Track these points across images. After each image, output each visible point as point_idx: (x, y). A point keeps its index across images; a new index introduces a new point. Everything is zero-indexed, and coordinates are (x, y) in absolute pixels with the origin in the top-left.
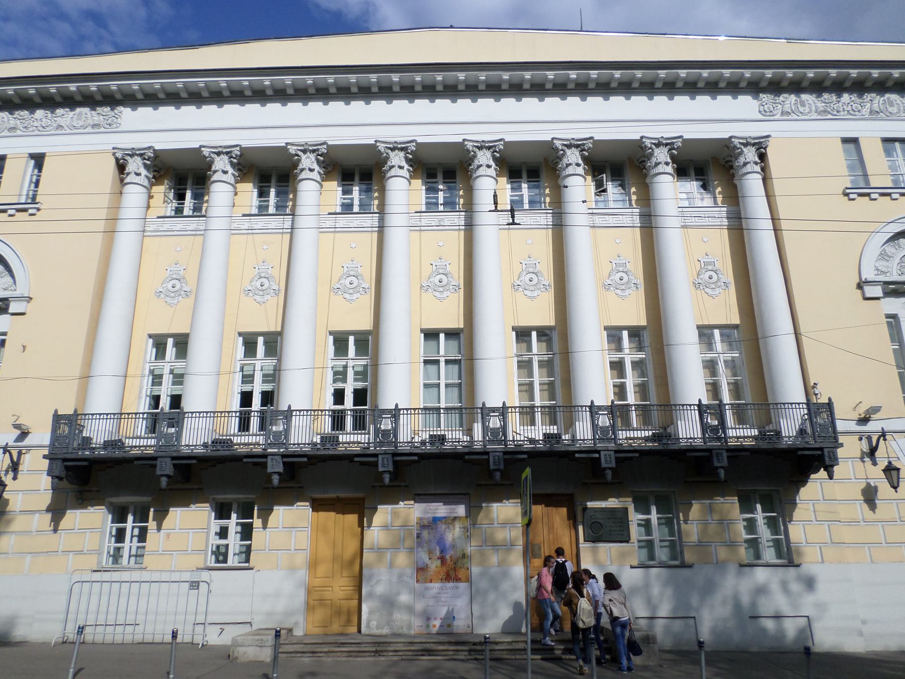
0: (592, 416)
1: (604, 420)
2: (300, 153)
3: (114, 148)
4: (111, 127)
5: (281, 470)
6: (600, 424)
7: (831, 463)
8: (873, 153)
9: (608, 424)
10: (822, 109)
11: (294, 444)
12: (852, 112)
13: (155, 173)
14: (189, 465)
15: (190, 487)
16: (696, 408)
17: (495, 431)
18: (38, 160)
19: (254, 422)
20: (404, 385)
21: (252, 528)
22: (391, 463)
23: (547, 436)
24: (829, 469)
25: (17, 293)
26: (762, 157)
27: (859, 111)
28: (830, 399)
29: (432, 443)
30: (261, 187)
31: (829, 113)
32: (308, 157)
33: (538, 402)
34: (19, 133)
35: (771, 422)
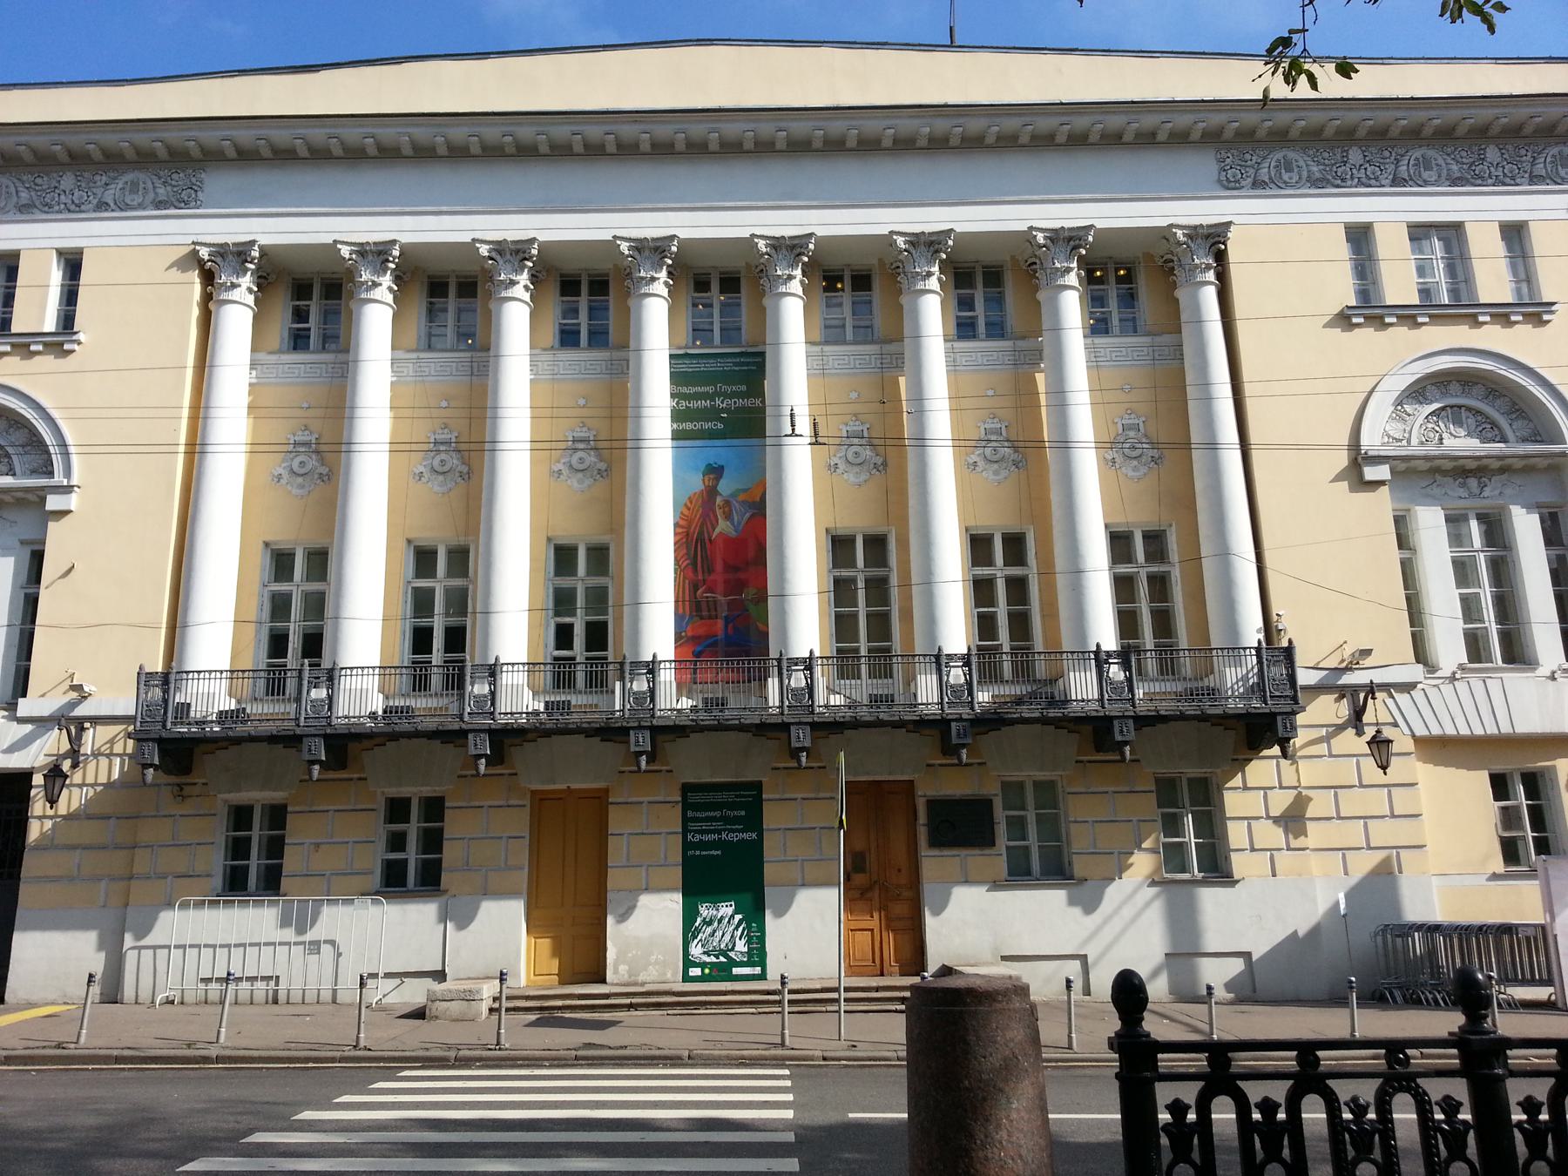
6: (952, 681)
8: (1392, 247)
10: (1318, 175)
15: (346, 776)
19: (436, 680)
23: (875, 700)
24: (1284, 743)
26: (1221, 257)
35: (1212, 672)
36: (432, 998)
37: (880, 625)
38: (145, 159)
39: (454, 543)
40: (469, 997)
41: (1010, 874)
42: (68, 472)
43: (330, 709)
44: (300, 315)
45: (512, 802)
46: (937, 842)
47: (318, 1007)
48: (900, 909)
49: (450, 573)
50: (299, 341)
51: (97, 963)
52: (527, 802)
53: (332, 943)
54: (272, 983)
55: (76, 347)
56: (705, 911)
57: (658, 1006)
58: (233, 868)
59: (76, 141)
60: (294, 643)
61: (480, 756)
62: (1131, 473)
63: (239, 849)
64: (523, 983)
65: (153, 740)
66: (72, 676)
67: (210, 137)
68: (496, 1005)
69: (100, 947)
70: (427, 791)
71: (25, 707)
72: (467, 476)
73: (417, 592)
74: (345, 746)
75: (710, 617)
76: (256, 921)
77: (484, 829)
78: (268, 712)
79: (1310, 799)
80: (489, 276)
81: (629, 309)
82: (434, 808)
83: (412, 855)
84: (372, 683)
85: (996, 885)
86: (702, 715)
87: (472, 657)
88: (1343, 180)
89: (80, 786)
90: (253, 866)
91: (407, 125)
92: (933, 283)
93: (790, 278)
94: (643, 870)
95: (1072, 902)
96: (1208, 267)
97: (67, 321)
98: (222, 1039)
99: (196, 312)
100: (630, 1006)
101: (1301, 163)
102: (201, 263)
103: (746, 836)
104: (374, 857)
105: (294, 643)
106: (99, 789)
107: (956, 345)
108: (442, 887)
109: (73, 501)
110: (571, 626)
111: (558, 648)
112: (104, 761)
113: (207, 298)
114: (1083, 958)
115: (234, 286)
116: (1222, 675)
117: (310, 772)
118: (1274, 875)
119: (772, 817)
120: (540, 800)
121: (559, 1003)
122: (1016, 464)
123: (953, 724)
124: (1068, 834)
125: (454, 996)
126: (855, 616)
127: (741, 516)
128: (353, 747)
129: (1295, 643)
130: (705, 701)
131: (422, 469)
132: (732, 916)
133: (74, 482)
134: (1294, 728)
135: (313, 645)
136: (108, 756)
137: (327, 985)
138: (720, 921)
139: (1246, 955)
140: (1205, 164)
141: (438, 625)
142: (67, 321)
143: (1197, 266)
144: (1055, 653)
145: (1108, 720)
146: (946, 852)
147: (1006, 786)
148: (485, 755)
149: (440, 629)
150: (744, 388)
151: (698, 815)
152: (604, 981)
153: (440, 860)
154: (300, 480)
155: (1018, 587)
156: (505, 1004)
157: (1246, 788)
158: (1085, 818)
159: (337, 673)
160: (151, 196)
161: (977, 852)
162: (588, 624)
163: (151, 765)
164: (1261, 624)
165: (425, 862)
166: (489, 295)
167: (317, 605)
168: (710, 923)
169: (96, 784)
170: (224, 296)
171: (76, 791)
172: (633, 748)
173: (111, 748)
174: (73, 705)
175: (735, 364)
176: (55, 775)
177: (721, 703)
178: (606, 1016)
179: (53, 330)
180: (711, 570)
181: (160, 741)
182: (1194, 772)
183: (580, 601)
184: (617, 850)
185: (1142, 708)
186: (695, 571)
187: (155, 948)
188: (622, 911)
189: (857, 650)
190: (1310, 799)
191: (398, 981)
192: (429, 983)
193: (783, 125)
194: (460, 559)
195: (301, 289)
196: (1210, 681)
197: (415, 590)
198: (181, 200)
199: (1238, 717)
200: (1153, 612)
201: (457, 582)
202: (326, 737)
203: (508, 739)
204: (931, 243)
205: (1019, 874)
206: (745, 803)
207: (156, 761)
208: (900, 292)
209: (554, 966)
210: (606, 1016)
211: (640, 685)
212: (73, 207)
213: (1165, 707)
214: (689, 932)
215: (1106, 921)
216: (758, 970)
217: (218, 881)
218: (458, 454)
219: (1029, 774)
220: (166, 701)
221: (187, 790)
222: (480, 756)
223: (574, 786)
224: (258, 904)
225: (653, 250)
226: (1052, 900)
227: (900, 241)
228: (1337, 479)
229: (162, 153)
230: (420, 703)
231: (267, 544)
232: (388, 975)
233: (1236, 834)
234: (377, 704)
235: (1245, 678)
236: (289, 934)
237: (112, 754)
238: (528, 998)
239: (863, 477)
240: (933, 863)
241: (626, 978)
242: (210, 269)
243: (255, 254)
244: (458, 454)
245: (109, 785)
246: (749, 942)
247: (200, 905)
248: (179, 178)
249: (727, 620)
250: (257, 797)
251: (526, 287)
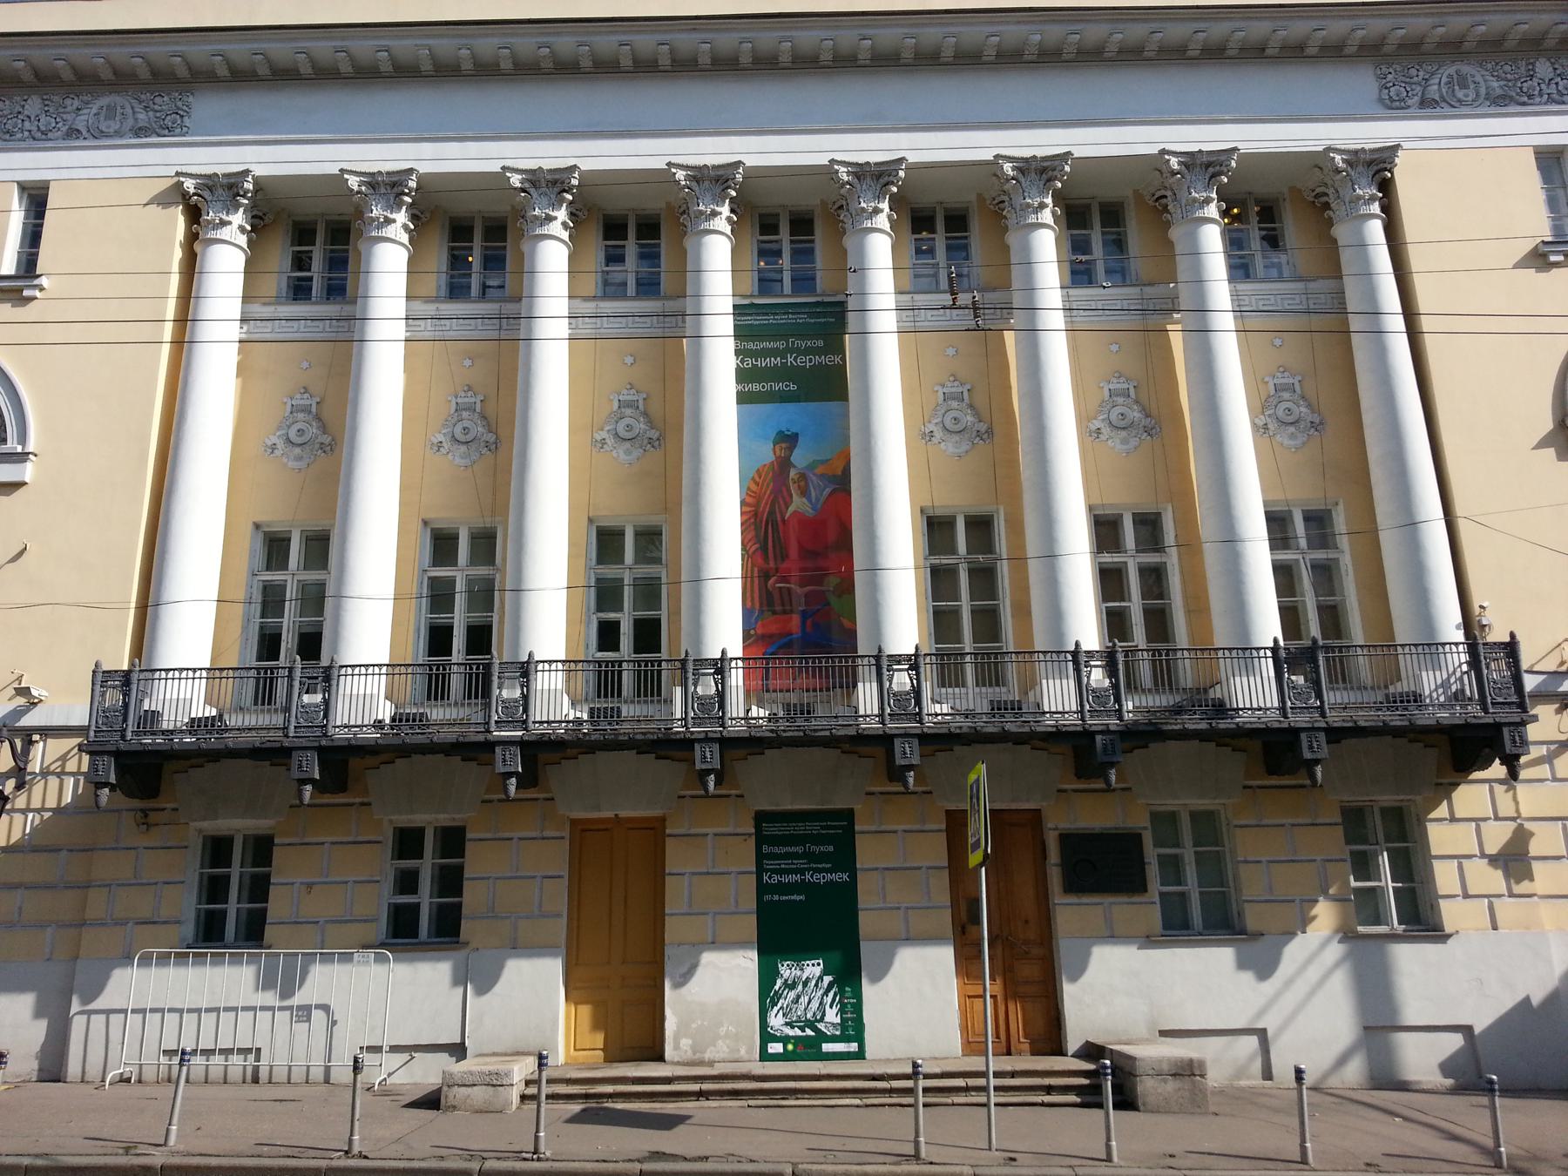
0: (1077, 670)
1: (901, 680)
7: (1515, 751)
9: (908, 687)
10: (1499, 92)
11: (541, 723)
12: (1555, 96)
13: (256, 221)
16: (1269, 653)
17: (704, 702)
19: (456, 683)
21: (269, 883)
24: (1511, 762)
26: (1386, 187)
28: (1512, 635)
30: (453, 249)
31: (1511, 99)
35: (1399, 679)
36: (450, 1082)
37: (988, 624)
38: (121, 80)
39: (479, 523)
40: (495, 1082)
41: (1165, 927)
42: (23, 439)
43: (326, 716)
44: (301, 262)
45: (547, 833)
46: (1075, 885)
47: (307, 1089)
48: (1029, 970)
49: (474, 560)
50: (299, 291)
51: (38, 1031)
52: (566, 834)
53: (326, 1008)
54: (251, 1057)
55: (37, 293)
56: (786, 971)
57: (735, 1094)
58: (210, 913)
59: (42, 56)
60: (288, 642)
61: (509, 775)
62: (1286, 442)
63: (215, 889)
64: (561, 1059)
65: (108, 753)
66: (20, 679)
67: (199, 52)
68: (532, 1090)
69: (38, 1013)
70: (444, 819)
72: (494, 446)
73: (433, 581)
74: (344, 763)
75: (785, 612)
76: (229, 981)
77: (516, 865)
78: (251, 722)
79: (1532, 834)
80: (520, 213)
81: (684, 252)
82: (453, 840)
83: (425, 899)
84: (376, 685)
85: (1149, 941)
86: (782, 725)
87: (500, 653)
88: (1530, 97)
89: (24, 812)
90: (232, 914)
91: (428, 37)
92: (1047, 216)
93: (877, 211)
94: (709, 919)
95: (1242, 964)
96: (1372, 199)
97: (29, 265)
98: (172, 1140)
99: (178, 254)
100: (700, 1095)
101: (1478, 78)
102: (185, 196)
103: (835, 877)
104: (380, 899)
105: (288, 642)
106: (47, 815)
107: (1071, 292)
108: (463, 937)
109: (28, 472)
110: (617, 624)
111: (601, 649)
112: (53, 782)
113: (192, 238)
114: (1262, 1034)
115: (224, 223)
116: (1417, 679)
117: (300, 793)
118: (1495, 928)
119: (867, 853)
120: (582, 831)
121: (609, 1089)
122: (1148, 431)
123: (1098, 738)
124: (1236, 877)
125: (477, 1080)
126: (956, 612)
127: (820, 492)
128: (355, 763)
129: (1519, 637)
130: (787, 707)
131: (441, 438)
133: (30, 449)
135: (310, 645)
136: (59, 775)
137: (318, 1061)
138: (805, 984)
139: (1467, 1030)
140: (1362, 81)
141: (460, 619)
142: (29, 265)
143: (1359, 198)
144: (1205, 651)
145: (1294, 732)
146: (1085, 900)
147: (1155, 816)
148: (516, 774)
149: (460, 623)
150: (820, 343)
151: (776, 850)
152: (660, 1058)
153: (459, 905)
154: (297, 450)
155: (1154, 578)
156: (546, 1090)
157: (1453, 819)
158: (1260, 852)
159: (335, 672)
160: (130, 122)
161: (1125, 899)
162: (636, 621)
163: (106, 784)
164: (1459, 620)
165: (441, 907)
166: (521, 234)
167: (316, 599)
168: (792, 986)
169: (43, 809)
170: (212, 235)
171: (18, 817)
172: (699, 766)
173: (63, 766)
174: (19, 713)
175: (811, 315)
177: (807, 711)
178: (670, 1108)
179: (12, 272)
180: (784, 556)
181: (118, 755)
182: (1388, 799)
183: (628, 593)
184: (677, 893)
185: (1335, 718)
186: (766, 558)
187: (108, 1012)
188: (684, 970)
190: (1532, 834)
191: (406, 1056)
192: (444, 1061)
193: (870, 32)
194: (486, 544)
195: (303, 233)
196: (1403, 687)
197: (433, 580)
198: (164, 128)
199: (1439, 729)
200: (1321, 609)
201: (482, 571)
202: (321, 750)
203: (545, 753)
204: (1043, 171)
205: (1177, 927)
206: (835, 836)
207: (113, 779)
208: (1006, 229)
209: (599, 1040)
210: (670, 1108)
211: (707, 687)
212: (39, 135)
213: (1365, 718)
214: (767, 997)
215: (1289, 983)
216: (854, 1047)
217: (189, 930)
218: (483, 428)
219: (1185, 802)
220: (126, 705)
221: (153, 817)
222: (509, 775)
223: (623, 814)
224: (236, 960)
225: (715, 179)
226: (1219, 958)
227: (1008, 168)
228: (1542, 444)
229: (144, 73)
230: (436, 713)
231: (257, 526)
232: (395, 1049)
233: (1445, 877)
234: (385, 712)
235: (1445, 685)
236: (270, 998)
237: (64, 773)
238: (569, 1081)
239: (964, 447)
240: (1070, 913)
241: (689, 1055)
242: (197, 205)
243: (249, 186)
244: (483, 428)
245: (58, 811)
246: (842, 1011)
247: (163, 960)
248: (164, 103)
249: (804, 614)
250: (237, 825)
251: (564, 224)
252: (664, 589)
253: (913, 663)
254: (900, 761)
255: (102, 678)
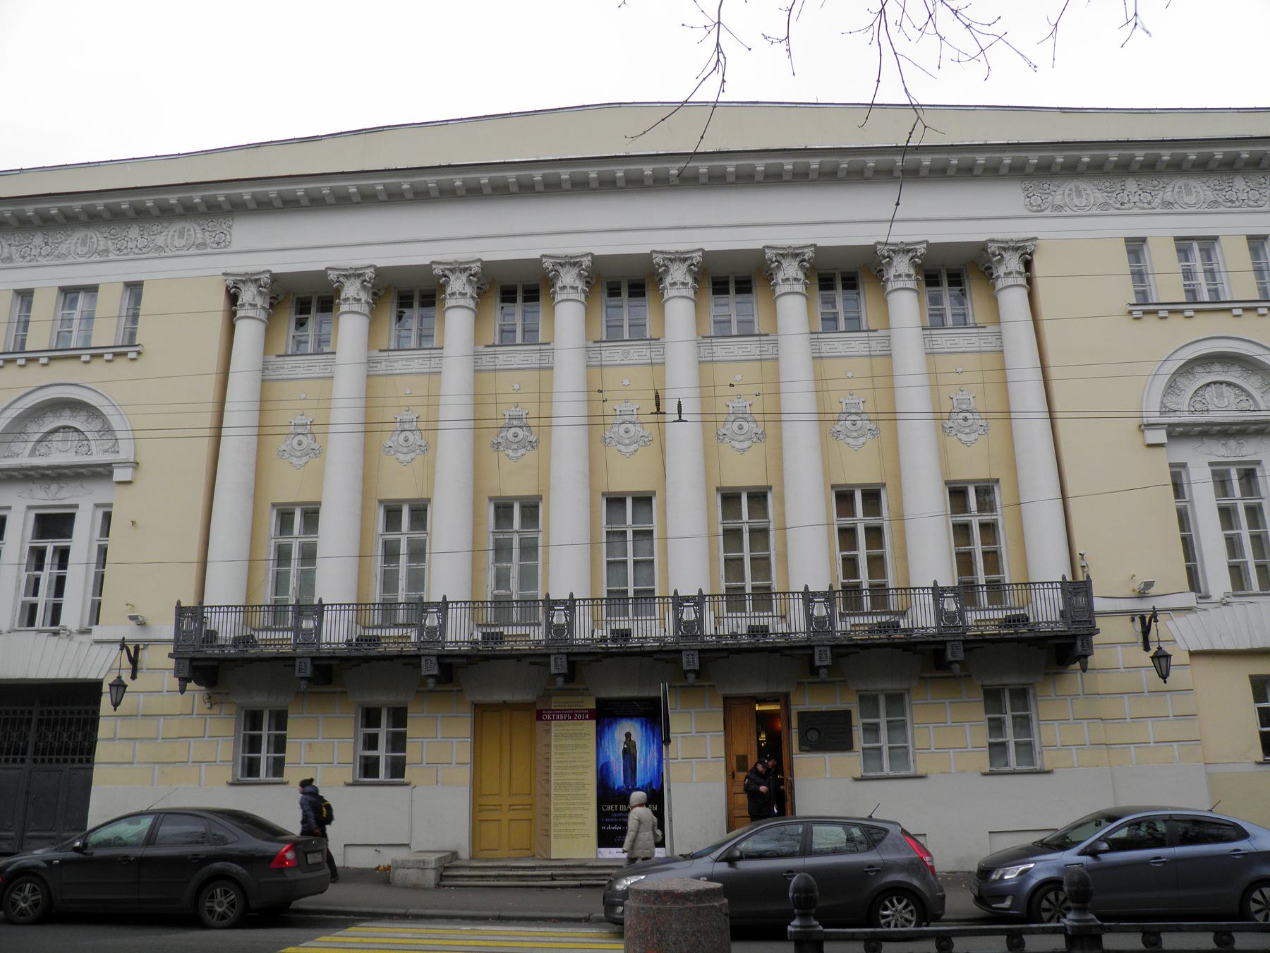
1: (820, 610)
2: (341, 279)
3: (224, 274)
4: (221, 246)
5: (436, 672)
8: (1162, 259)
10: (1102, 201)
14: (330, 666)
15: (333, 690)
18: (134, 288)
20: (925, 555)
22: (565, 664)
23: (753, 631)
25: (122, 457)
26: (1028, 265)
27: (1149, 203)
29: (614, 640)
32: (457, 278)
33: (401, 596)
34: (209, 250)
46: (809, 746)
71: (98, 632)
125: (410, 865)
132: (288, 630)
134: (1090, 646)
176: (119, 686)
189: (743, 588)
252: (540, 549)
253: (829, 596)
254: (817, 663)
255: (180, 611)
